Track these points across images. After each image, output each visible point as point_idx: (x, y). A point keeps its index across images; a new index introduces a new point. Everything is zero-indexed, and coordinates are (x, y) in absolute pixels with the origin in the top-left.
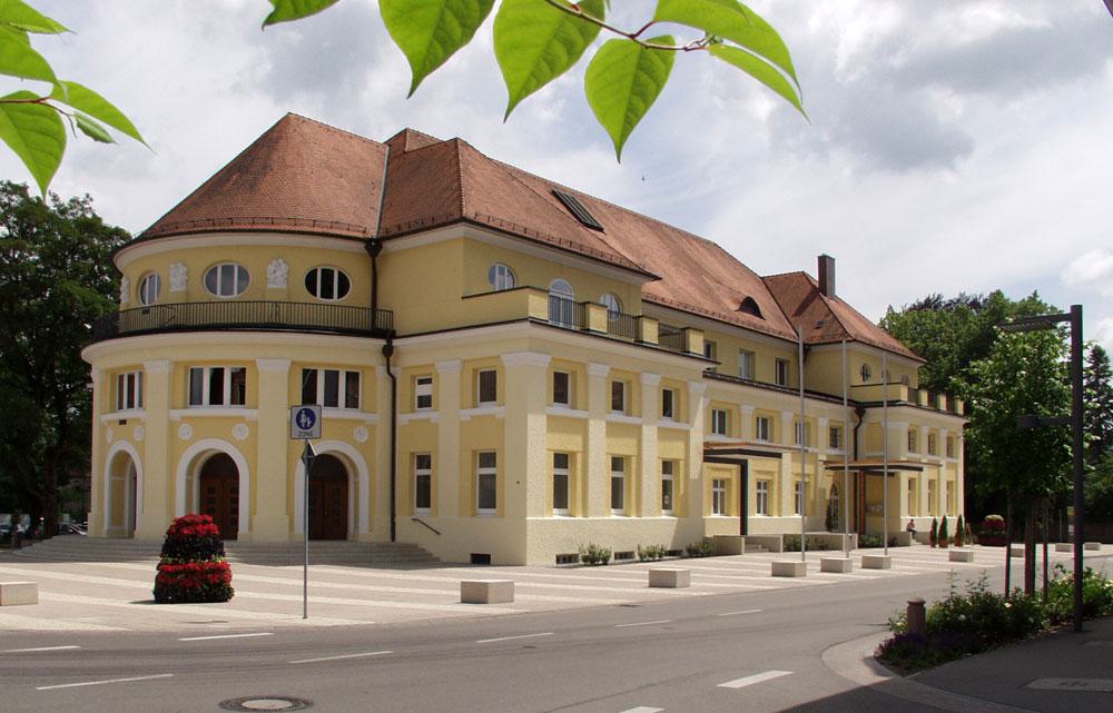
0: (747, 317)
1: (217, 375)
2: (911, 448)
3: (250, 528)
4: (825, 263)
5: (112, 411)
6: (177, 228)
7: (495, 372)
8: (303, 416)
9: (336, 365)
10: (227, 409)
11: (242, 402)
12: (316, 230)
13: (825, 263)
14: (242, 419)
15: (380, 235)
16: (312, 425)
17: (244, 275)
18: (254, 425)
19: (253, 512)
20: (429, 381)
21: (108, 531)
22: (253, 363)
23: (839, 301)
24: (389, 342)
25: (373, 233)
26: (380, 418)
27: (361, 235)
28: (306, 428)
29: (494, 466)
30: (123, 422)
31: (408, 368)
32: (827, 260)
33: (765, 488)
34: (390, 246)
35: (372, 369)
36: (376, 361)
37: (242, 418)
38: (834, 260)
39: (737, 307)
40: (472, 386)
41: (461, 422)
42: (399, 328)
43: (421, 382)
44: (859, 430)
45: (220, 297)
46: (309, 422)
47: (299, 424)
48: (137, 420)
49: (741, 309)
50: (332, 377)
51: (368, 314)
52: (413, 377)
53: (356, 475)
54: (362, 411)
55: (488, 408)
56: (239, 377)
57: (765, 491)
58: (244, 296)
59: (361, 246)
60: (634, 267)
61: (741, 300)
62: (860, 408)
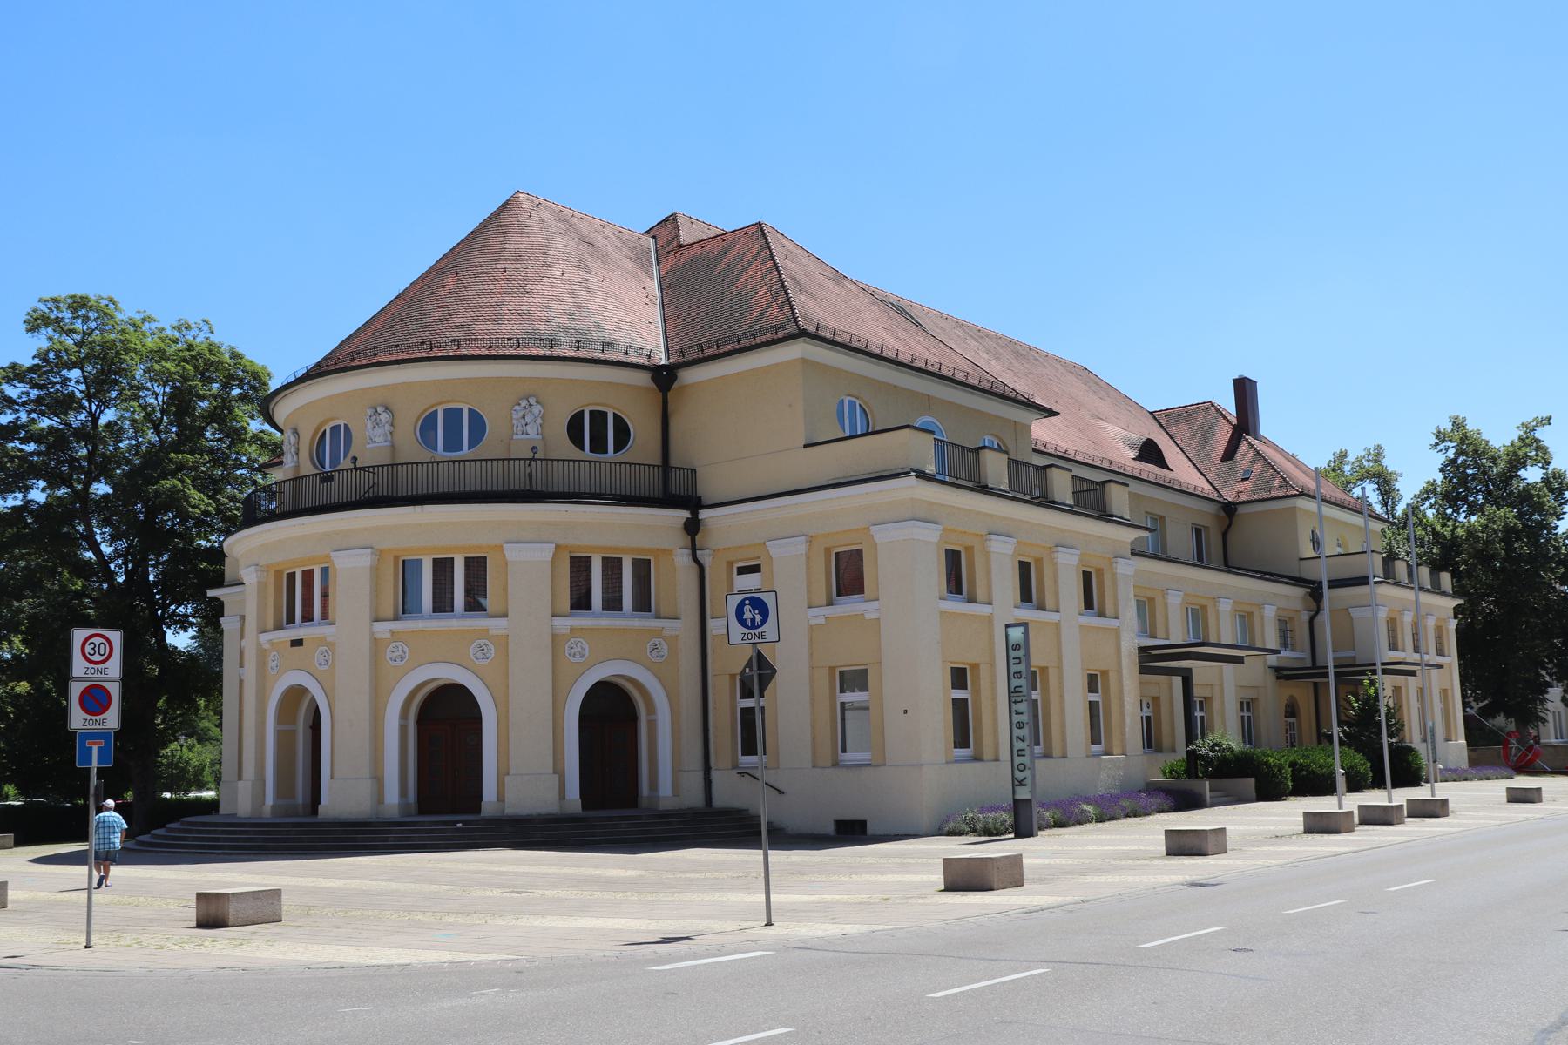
0: (1149, 470)
1: (612, 566)
2: (1393, 646)
4: (1244, 390)
5: (278, 627)
6: (353, 359)
7: (859, 553)
8: (747, 608)
9: (616, 549)
10: (459, 622)
12: (582, 354)
13: (1244, 390)
14: (484, 633)
15: (672, 360)
16: (763, 622)
17: (477, 422)
18: (503, 643)
19: (503, 774)
20: (756, 569)
21: (273, 806)
23: (1265, 441)
24: (695, 514)
25: (661, 359)
26: (685, 629)
27: (645, 361)
28: (753, 626)
30: (297, 643)
32: (1247, 382)
33: (1248, 710)
34: (689, 376)
35: (667, 552)
38: (1256, 382)
39: (1134, 454)
40: (822, 576)
41: (811, 628)
42: (709, 487)
43: (743, 571)
44: (1315, 621)
45: (441, 453)
46: (758, 618)
47: (742, 622)
48: (322, 641)
49: (1140, 458)
50: (612, 566)
51: (658, 473)
52: (730, 564)
53: (651, 709)
54: (658, 617)
55: (849, 606)
57: (1202, 714)
58: (480, 452)
59: (644, 379)
60: (1020, 397)
61: (1140, 443)
62: (1315, 591)
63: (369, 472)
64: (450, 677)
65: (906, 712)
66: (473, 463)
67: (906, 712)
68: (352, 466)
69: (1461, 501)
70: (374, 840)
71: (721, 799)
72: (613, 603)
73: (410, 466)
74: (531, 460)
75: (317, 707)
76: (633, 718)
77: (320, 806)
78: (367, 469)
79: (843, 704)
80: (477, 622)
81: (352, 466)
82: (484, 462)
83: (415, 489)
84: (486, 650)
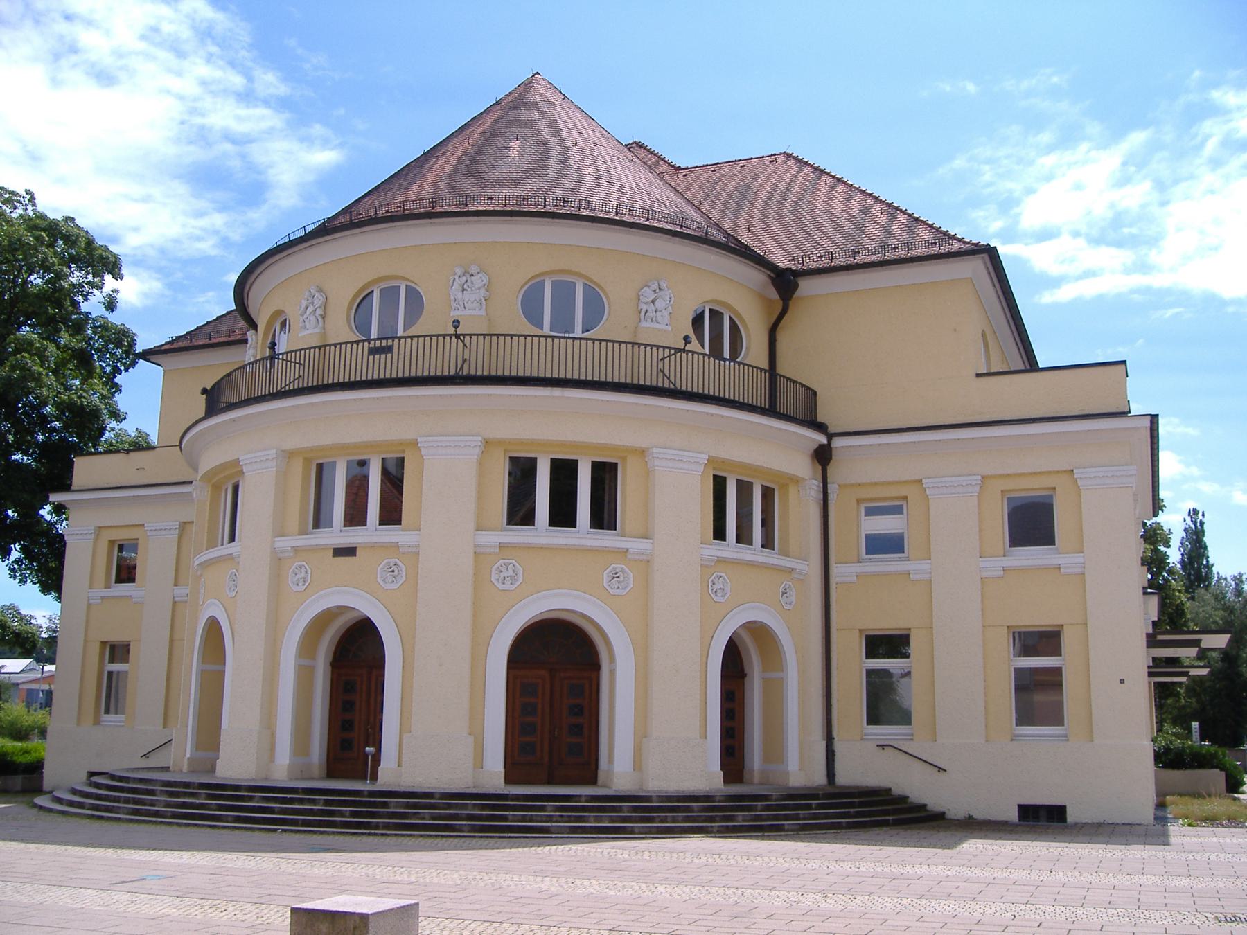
1: (564, 472)
3: (638, 765)
11: (398, 521)
17: (415, 301)
19: (404, 729)
22: (414, 444)
29: (127, 661)
31: (846, 486)
35: (796, 480)
36: (801, 466)
37: (396, 546)
56: (605, 475)
63: (283, 360)
64: (364, 612)
66: (508, 338)
68: (452, 331)
70: (373, 815)
71: (847, 776)
72: (563, 515)
74: (677, 350)
76: (595, 666)
77: (379, 768)
78: (281, 357)
79: (110, 674)
80: (603, 538)
81: (452, 331)
82: (522, 339)
84: (396, 572)
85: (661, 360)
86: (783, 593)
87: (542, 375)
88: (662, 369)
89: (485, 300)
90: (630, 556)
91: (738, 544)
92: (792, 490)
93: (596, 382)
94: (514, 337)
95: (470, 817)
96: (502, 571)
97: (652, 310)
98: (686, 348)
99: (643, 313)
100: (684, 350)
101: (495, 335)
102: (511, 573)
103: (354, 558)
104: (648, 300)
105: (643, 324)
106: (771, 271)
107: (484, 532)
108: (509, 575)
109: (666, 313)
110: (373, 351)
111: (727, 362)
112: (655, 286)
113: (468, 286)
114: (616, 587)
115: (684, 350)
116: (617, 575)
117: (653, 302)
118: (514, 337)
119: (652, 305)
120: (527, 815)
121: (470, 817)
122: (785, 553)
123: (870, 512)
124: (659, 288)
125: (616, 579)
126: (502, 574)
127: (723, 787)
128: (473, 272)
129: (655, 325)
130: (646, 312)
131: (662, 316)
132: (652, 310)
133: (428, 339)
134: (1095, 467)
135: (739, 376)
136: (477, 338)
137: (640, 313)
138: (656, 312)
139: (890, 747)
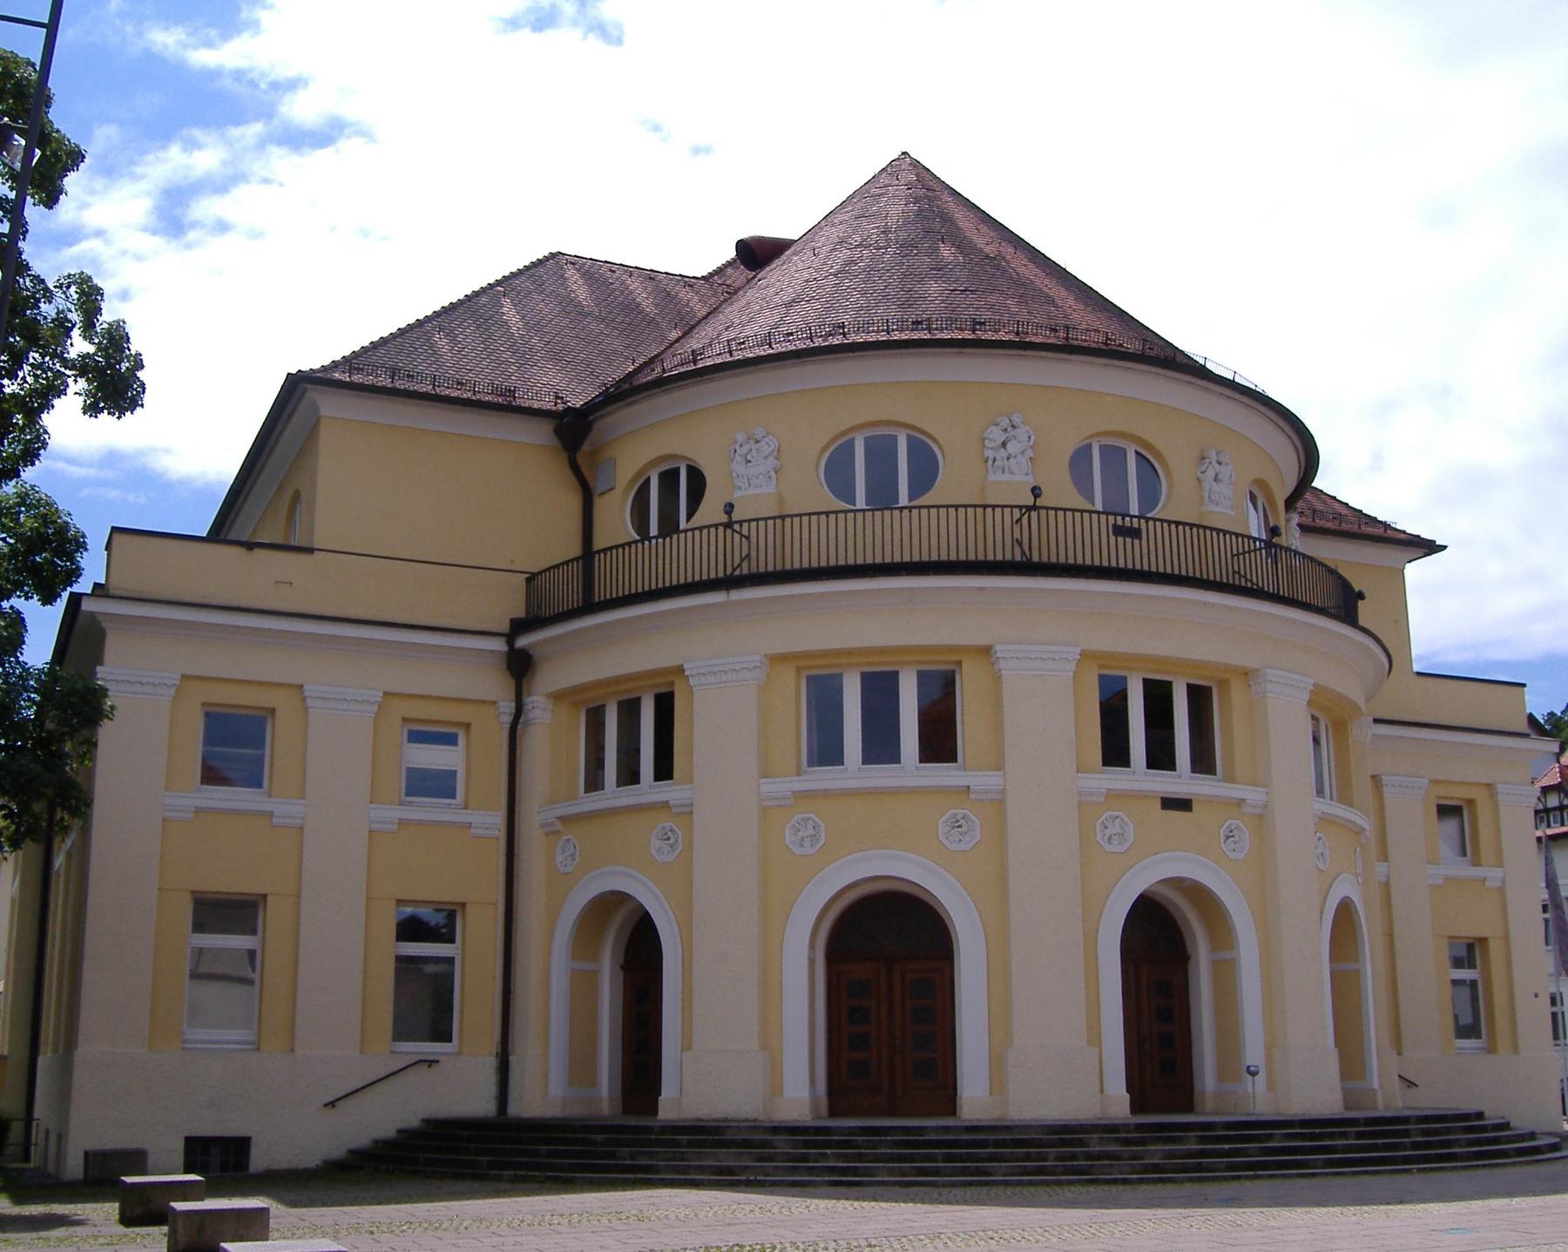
22: (680, 670)
65: (1536, 995)
67: (1536, 995)
68: (724, 518)
69: (31, 719)
73: (762, 523)
74: (1029, 509)
75: (1161, 881)
77: (660, 1098)
80: (940, 774)
81: (724, 518)
83: (878, 550)
84: (672, 841)
85: (1017, 522)
86: (1228, 837)
87: (935, 558)
88: (1019, 538)
89: (776, 472)
90: (972, 796)
91: (1148, 771)
92: (1236, 690)
93: (963, 563)
94: (960, 509)
95: (831, 1170)
96: (799, 830)
97: (1002, 457)
98: (1038, 504)
99: (990, 462)
100: (1034, 507)
101: (952, 506)
102: (811, 831)
103: (1190, 813)
104: (994, 444)
105: (992, 477)
106: (554, 418)
107: (1087, 775)
108: (1115, 832)
109: (1023, 460)
110: (1119, 531)
111: (654, 541)
112: (1005, 423)
113: (753, 457)
114: (957, 840)
115: (1034, 507)
116: (957, 825)
117: (1004, 445)
118: (960, 509)
119: (1002, 450)
120: (969, 1167)
121: (831, 1170)
122: (1230, 779)
123: (417, 737)
124: (1013, 426)
125: (956, 829)
126: (799, 833)
127: (1130, 1116)
128: (759, 437)
129: (1007, 477)
130: (995, 460)
131: (1017, 463)
132: (1002, 457)
133: (697, 532)
134: (1041, 644)
135: (605, 564)
136: (938, 512)
137: (986, 462)
138: (1008, 459)
139: (422, 1063)
